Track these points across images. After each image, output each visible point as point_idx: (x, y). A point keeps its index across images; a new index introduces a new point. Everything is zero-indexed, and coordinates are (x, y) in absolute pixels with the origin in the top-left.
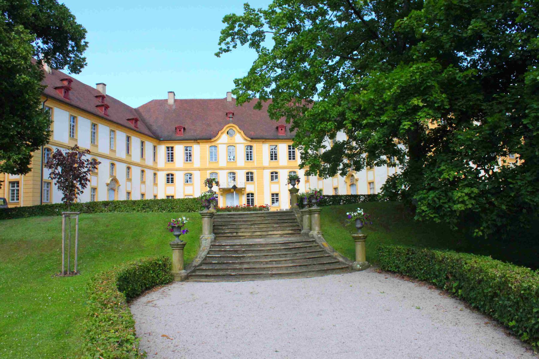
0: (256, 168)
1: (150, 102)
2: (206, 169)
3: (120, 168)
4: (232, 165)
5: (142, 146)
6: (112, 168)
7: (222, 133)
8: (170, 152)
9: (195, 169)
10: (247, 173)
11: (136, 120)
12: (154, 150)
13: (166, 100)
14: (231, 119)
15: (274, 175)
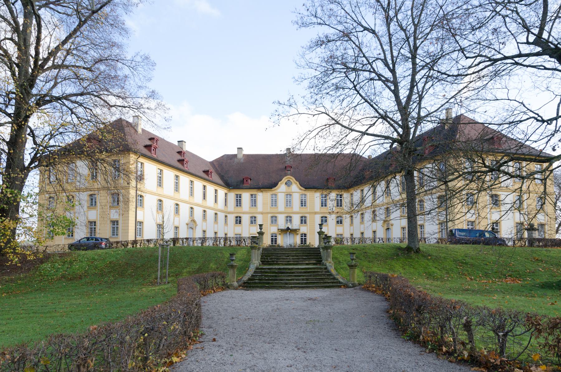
0: (309, 213)
1: (222, 157)
2: (268, 213)
4: (289, 210)
8: (239, 198)
9: (244, 213)
10: (302, 217)
15: (324, 219)
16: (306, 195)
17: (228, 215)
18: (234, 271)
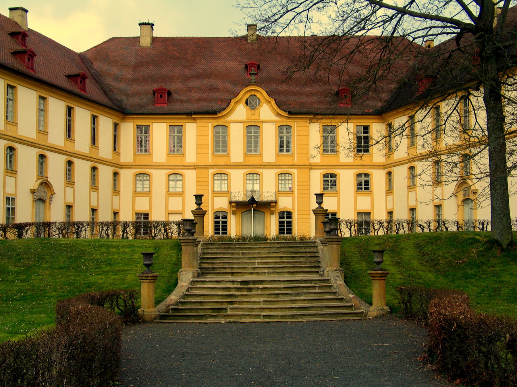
2: (207, 167)
3: (56, 164)
5: (115, 131)
6: (42, 164)
7: (237, 103)
11: (84, 77)
12: (94, 123)
13: (136, 39)
14: (253, 77)
15: (329, 179)
16: (289, 127)
17: (19, 147)
18: (329, 132)
